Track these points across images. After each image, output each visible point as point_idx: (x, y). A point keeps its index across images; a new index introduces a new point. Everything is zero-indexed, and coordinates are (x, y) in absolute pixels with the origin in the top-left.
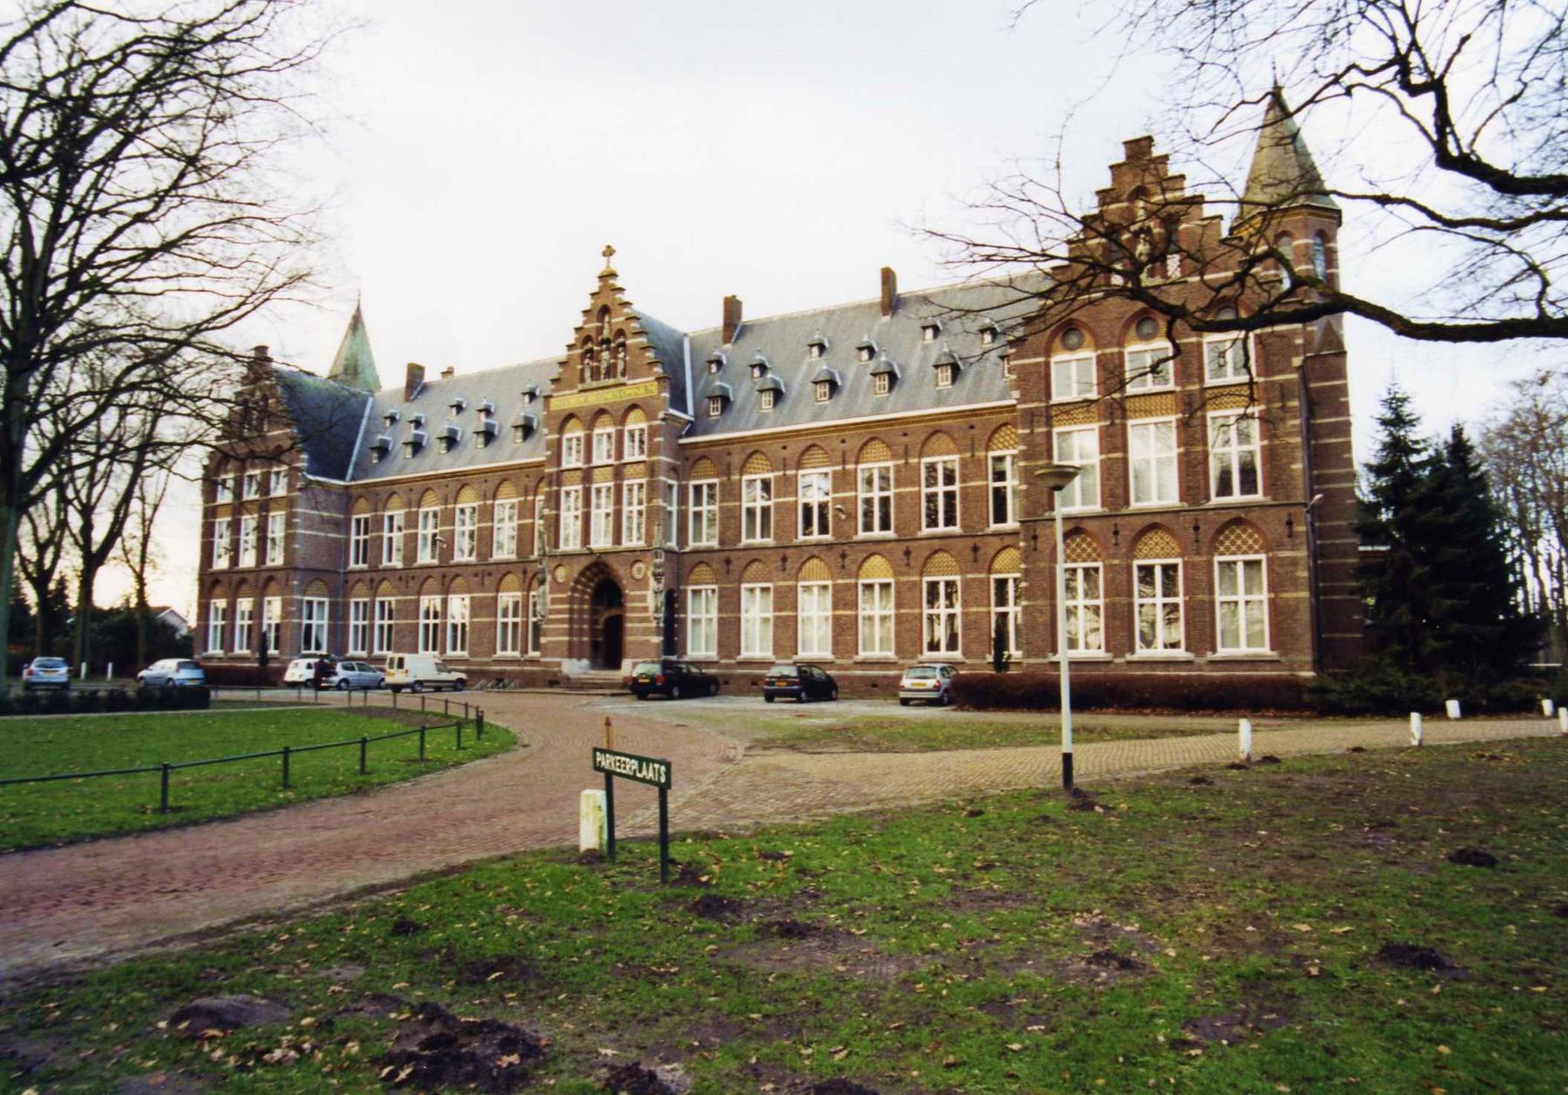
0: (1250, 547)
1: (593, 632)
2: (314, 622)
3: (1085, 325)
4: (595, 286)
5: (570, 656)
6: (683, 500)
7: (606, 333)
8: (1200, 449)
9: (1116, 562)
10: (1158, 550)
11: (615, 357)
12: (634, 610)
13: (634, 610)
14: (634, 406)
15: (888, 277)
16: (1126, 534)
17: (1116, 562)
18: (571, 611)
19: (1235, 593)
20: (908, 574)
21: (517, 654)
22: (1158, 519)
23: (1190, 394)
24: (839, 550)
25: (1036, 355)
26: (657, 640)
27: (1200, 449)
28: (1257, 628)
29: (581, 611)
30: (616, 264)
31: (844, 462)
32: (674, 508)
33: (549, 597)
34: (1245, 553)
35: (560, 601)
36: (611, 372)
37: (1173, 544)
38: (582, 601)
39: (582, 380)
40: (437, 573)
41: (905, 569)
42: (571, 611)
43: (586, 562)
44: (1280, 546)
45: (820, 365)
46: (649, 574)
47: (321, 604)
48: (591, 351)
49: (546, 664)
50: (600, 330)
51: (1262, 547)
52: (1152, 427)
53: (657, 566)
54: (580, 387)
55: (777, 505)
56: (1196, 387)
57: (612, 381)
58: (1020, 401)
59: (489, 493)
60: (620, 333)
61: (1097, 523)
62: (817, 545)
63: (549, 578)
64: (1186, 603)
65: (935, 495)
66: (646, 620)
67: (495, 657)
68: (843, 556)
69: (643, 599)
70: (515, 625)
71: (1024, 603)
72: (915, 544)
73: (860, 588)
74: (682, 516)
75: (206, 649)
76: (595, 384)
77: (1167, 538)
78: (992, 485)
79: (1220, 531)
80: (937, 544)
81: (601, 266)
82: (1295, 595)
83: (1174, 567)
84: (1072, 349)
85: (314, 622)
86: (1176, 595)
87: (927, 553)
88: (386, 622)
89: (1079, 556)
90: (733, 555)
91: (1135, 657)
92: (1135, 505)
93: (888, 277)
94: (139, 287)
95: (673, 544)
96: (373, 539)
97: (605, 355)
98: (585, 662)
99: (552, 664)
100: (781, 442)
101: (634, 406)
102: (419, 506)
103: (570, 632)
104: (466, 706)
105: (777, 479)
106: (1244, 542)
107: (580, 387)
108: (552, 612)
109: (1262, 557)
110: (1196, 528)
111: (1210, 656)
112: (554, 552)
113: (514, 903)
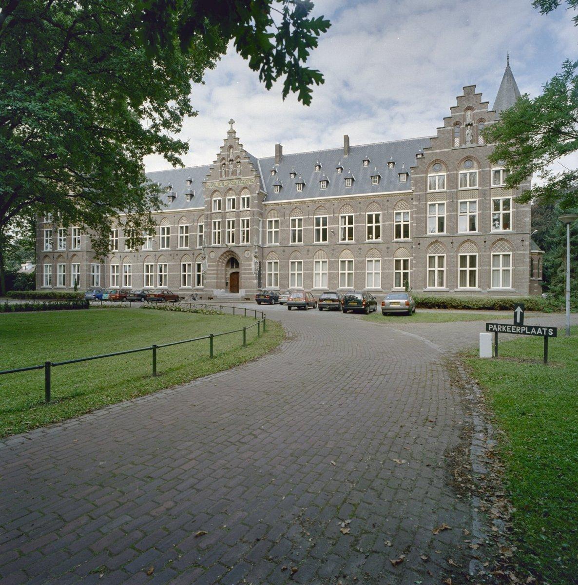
1: (226, 278)
2: (95, 274)
3: (443, 162)
4: (226, 137)
5: (217, 288)
6: (264, 227)
7: (231, 157)
8: (488, 212)
10: (432, 252)
11: (236, 167)
12: (246, 270)
13: (246, 270)
16: (456, 244)
18: (217, 270)
19: (499, 266)
20: (360, 257)
21: (190, 287)
22: (503, 237)
23: (485, 190)
24: (332, 247)
25: (422, 173)
26: (256, 281)
27: (488, 212)
29: (222, 270)
30: (235, 127)
31: (334, 213)
32: (261, 230)
33: (207, 265)
34: (439, 253)
35: (212, 266)
36: (234, 173)
37: (475, 247)
38: (222, 266)
39: (221, 176)
40: (153, 254)
41: (359, 255)
42: (217, 270)
44: (519, 249)
45: (188, 187)
46: (252, 255)
47: (98, 266)
49: (206, 291)
50: (228, 156)
54: (220, 179)
55: (190, 235)
56: (488, 188)
57: (234, 177)
58: (416, 191)
59: (176, 222)
60: (238, 157)
61: (445, 239)
62: (322, 245)
63: (207, 257)
64: (447, 270)
66: (251, 274)
67: (180, 288)
68: (333, 250)
69: (250, 265)
70: (117, 276)
71: (414, 269)
72: (311, 247)
73: (366, 261)
74: (264, 232)
75: (42, 285)
77: (473, 245)
79: (494, 243)
81: (228, 128)
83: (475, 256)
84: (436, 171)
85: (95, 274)
87: (368, 249)
89: (437, 251)
90: (286, 249)
91: (458, 290)
92: (460, 232)
93: (347, 139)
98: (223, 290)
99: (209, 291)
100: (307, 204)
101: (216, 191)
103: (217, 278)
104: (256, 311)
105: (305, 219)
106: (504, 247)
107: (220, 179)
108: (208, 270)
109: (510, 253)
110: (485, 242)
111: (488, 290)
112: (209, 246)
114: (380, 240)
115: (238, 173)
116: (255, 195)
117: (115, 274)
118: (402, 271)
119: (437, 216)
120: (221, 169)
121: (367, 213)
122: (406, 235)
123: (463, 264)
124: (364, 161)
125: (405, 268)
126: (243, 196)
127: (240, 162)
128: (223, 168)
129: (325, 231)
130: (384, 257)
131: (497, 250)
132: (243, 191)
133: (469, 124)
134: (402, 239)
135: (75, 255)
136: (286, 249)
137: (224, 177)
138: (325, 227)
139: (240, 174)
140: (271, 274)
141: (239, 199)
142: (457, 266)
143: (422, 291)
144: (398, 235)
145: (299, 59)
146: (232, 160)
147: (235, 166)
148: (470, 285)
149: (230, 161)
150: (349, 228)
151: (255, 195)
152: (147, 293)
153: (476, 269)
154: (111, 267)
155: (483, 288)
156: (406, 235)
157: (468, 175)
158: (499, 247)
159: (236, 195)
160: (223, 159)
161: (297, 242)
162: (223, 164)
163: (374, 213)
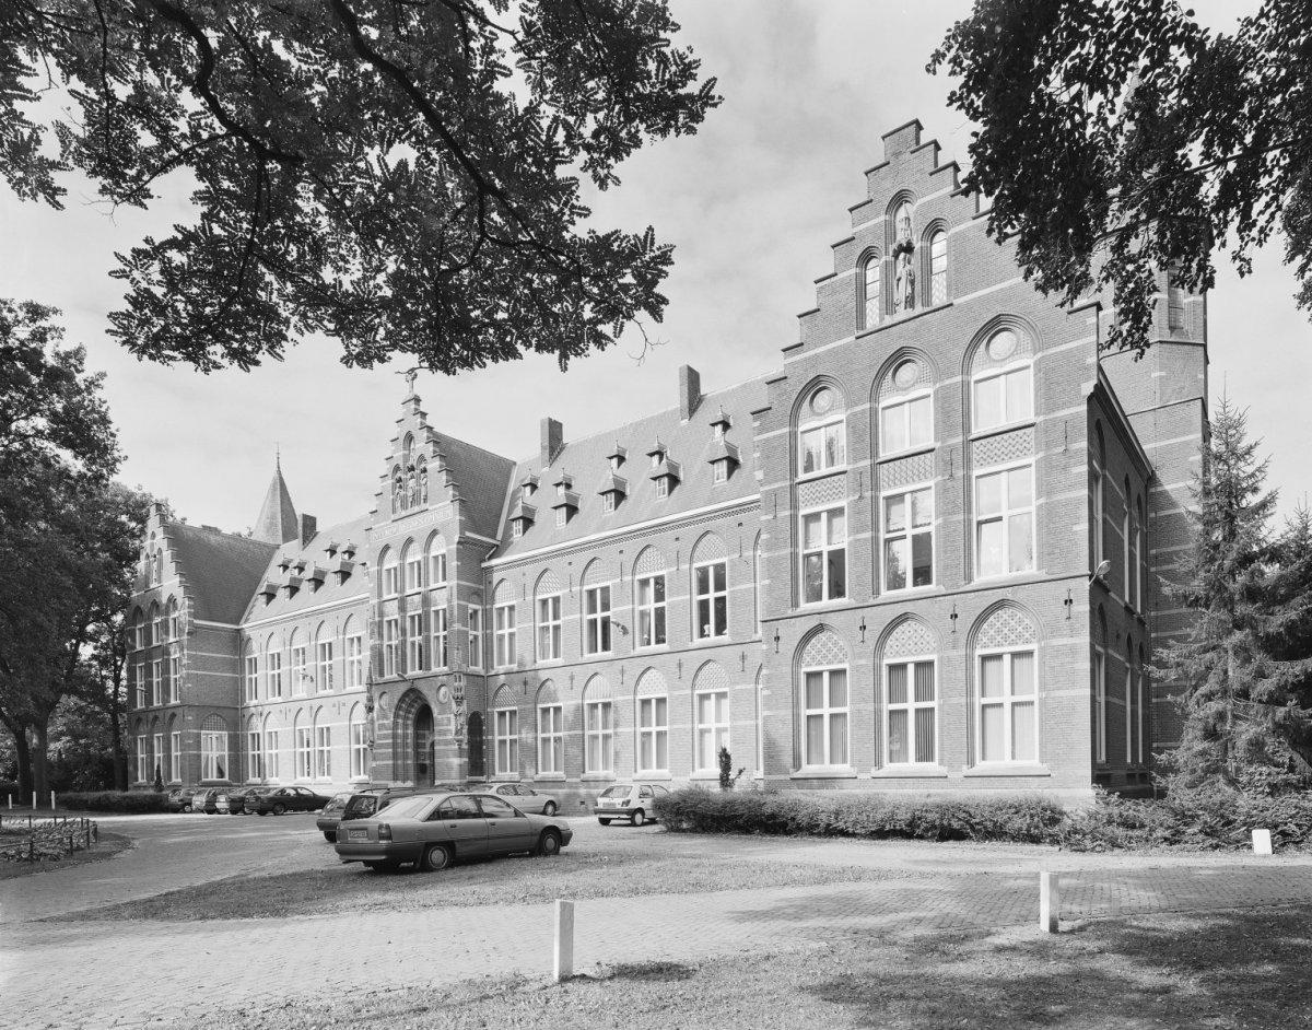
0: (1019, 636)
6: (488, 625)
9: (863, 662)
10: (992, 639)
16: (965, 621)
17: (863, 662)
22: (1007, 594)
28: (896, 747)
34: (1013, 643)
43: (403, 688)
44: (1055, 632)
48: (400, 480)
51: (1033, 635)
53: (458, 689)
57: (416, 509)
65: (603, 610)
76: (404, 513)
80: (707, 654)
82: (1073, 693)
86: (932, 699)
88: (305, 750)
95: (479, 669)
97: (412, 483)
107: (393, 517)
108: (380, 738)
113: (308, 1010)
114: (725, 638)
119: (910, 532)
131: (1006, 638)
134: (713, 639)
135: (820, 628)
138: (660, 605)
140: (650, 734)
143: (788, 777)
148: (919, 759)
154: (250, 738)
155: (951, 766)
158: (999, 631)
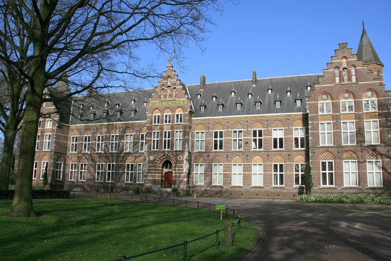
10: (330, 158)
14: (156, 109)
15: (255, 74)
25: (70, 117)
52: (371, 122)
57: (171, 99)
78: (214, 139)
93: (255, 74)
94: (124, 27)
96: (79, 144)
102: (125, 133)
115: (174, 95)
116: (186, 113)
117: (74, 170)
118: (278, 173)
120: (161, 93)
121: (253, 129)
122: (281, 146)
123: (276, 170)
124: (248, 94)
125: (281, 170)
126: (166, 114)
127: (175, 88)
128: (162, 92)
129: (221, 141)
130: (286, 162)
132: (178, 110)
133: (345, 68)
136: (269, 153)
137: (163, 98)
139: (175, 96)
141: (174, 115)
142: (319, 170)
144: (275, 147)
145: (56, 79)
146: (170, 87)
147: (172, 91)
149: (168, 87)
150: (259, 139)
151: (186, 113)
152: (340, 208)
153: (273, 173)
156: (281, 146)
157: (325, 104)
159: (172, 112)
160: (163, 85)
161: (218, 150)
162: (162, 89)
163: (257, 130)
